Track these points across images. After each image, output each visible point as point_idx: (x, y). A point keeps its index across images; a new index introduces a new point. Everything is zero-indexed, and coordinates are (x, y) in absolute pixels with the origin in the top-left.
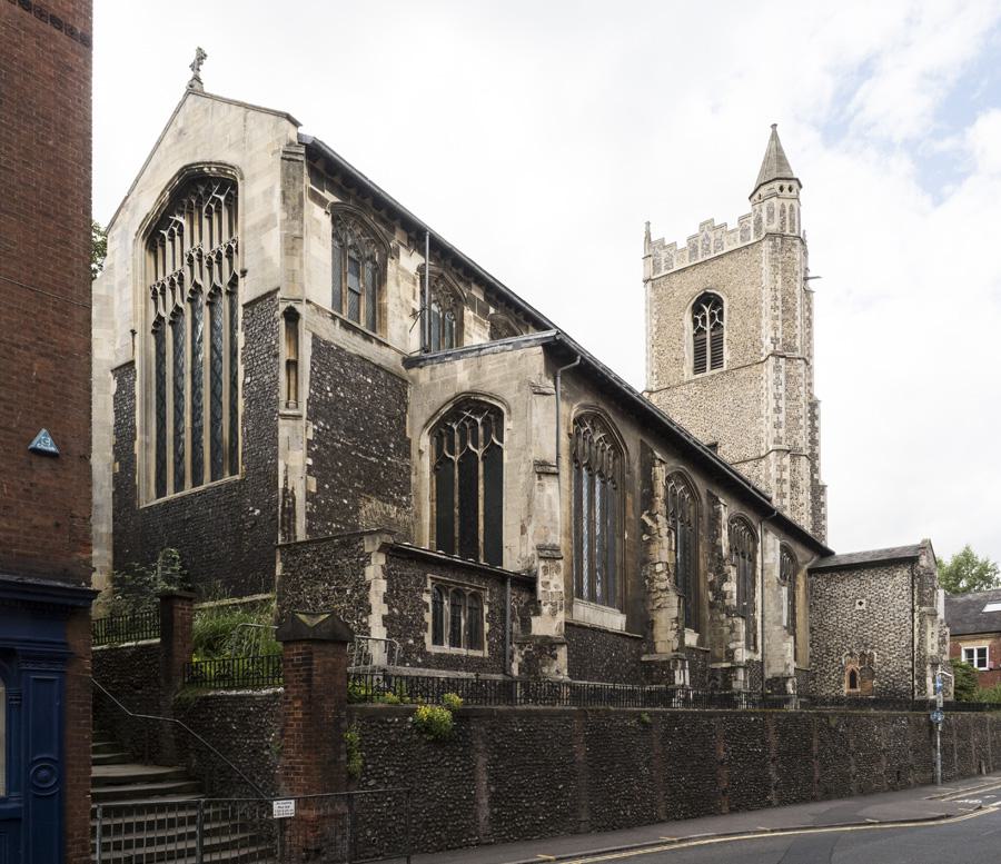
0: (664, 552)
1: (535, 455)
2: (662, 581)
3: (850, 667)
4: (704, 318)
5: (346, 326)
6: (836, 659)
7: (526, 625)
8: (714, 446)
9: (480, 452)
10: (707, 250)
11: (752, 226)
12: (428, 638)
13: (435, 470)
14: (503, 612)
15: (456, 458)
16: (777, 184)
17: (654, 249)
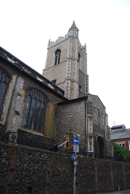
6: (63, 136)
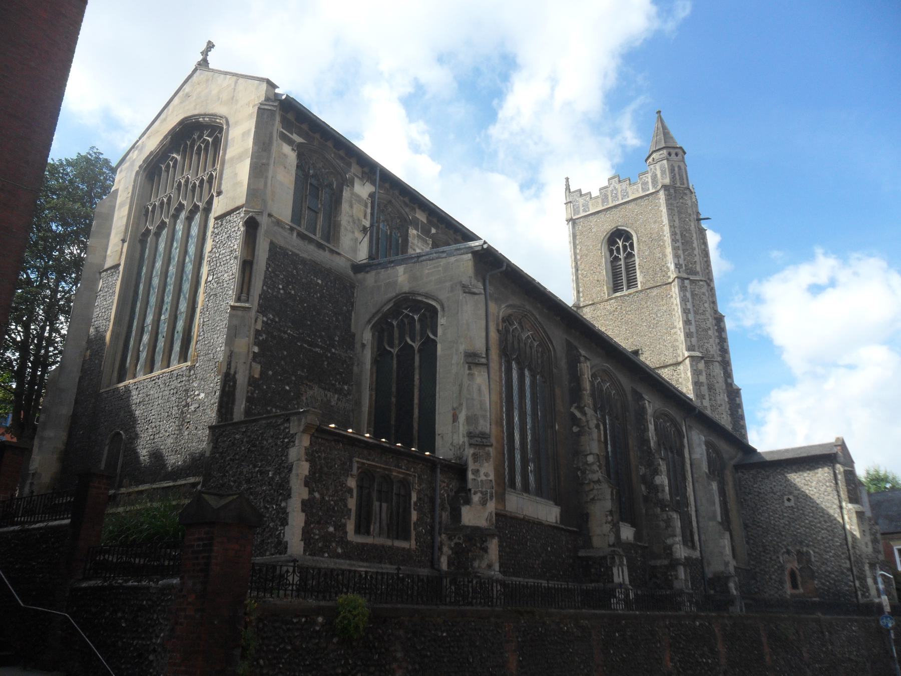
2: (594, 472)
4: (618, 249)
5: (301, 236)
6: (774, 557)
7: (456, 515)
8: (636, 353)
11: (650, 180)
12: (350, 527)
14: (432, 500)
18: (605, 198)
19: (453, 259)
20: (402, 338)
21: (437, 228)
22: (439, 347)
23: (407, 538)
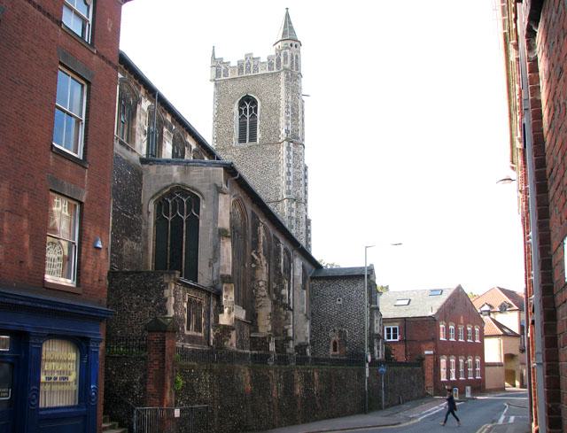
0: (263, 275)
1: (219, 226)
2: (262, 291)
3: (334, 338)
4: (246, 110)
9: (184, 218)
10: (249, 70)
13: (156, 223)
15: (170, 219)
16: (289, 42)
17: (219, 66)
18: (241, 69)
19: (211, 169)
20: (174, 212)
21: (123, 74)
22: (200, 221)
23: (201, 332)
